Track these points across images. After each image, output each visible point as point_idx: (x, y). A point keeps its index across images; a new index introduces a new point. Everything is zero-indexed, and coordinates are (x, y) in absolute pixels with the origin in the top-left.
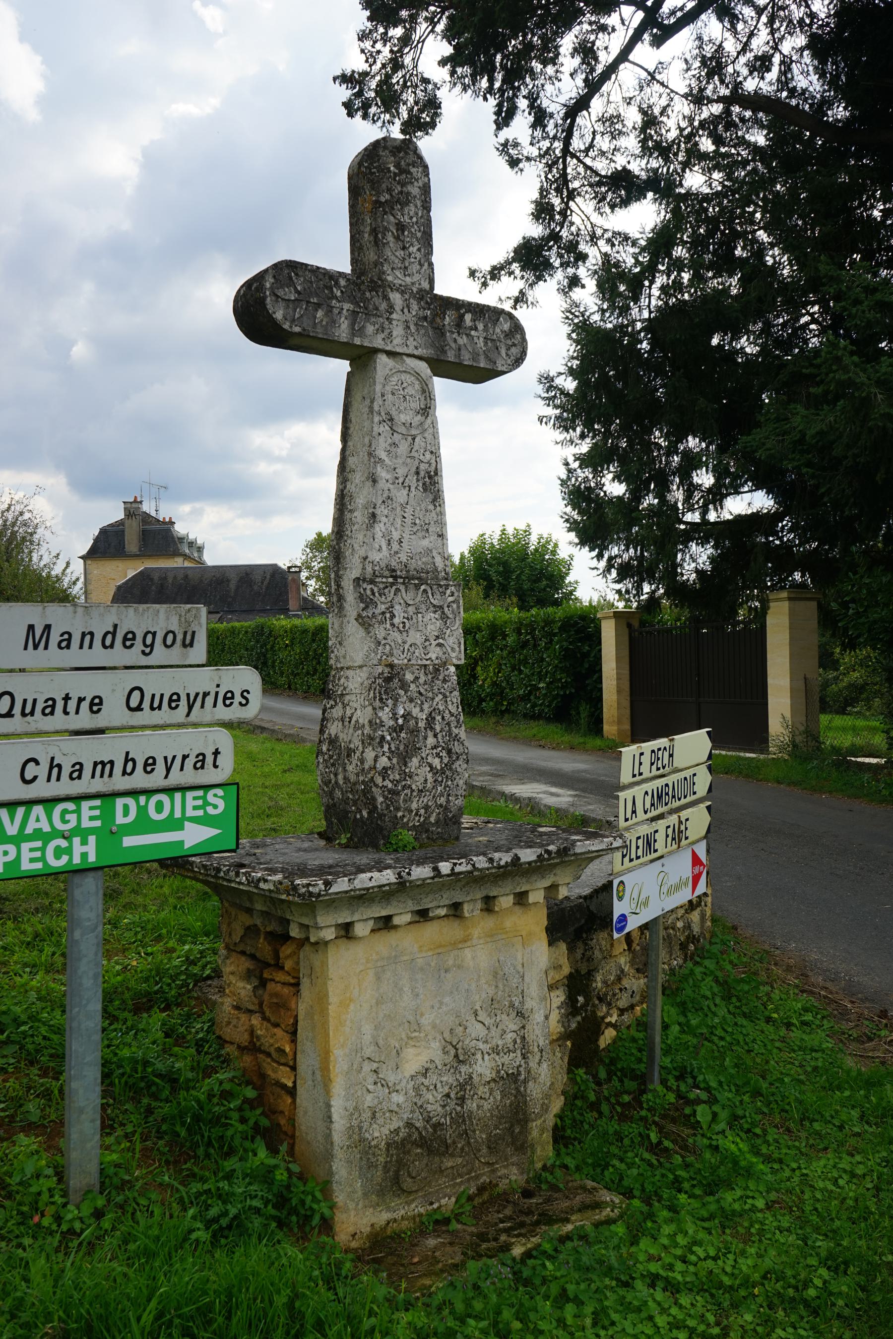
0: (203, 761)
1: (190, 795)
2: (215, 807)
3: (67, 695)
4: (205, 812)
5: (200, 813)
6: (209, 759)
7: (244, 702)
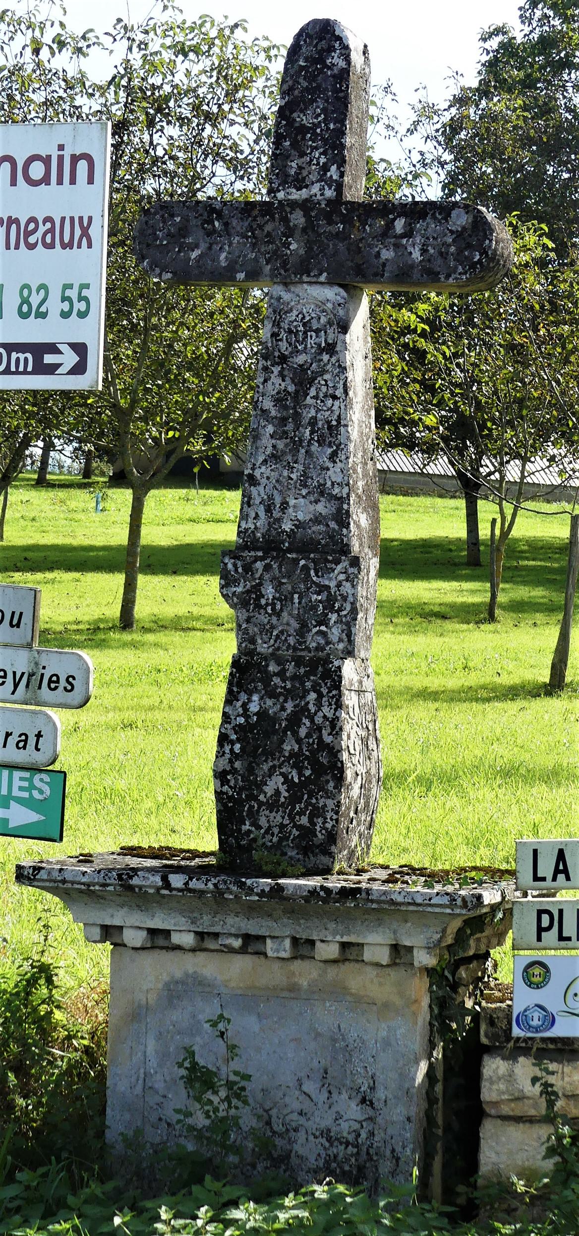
0: (26, 741)
1: (17, 774)
2: (41, 792)
3: (40, 732)
4: (31, 794)
5: (26, 795)
6: (32, 741)
7: (69, 687)
